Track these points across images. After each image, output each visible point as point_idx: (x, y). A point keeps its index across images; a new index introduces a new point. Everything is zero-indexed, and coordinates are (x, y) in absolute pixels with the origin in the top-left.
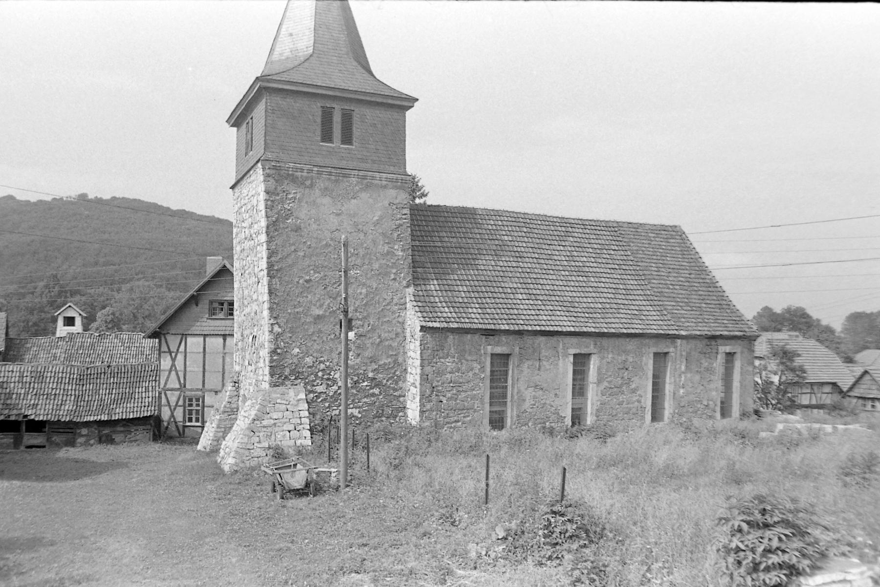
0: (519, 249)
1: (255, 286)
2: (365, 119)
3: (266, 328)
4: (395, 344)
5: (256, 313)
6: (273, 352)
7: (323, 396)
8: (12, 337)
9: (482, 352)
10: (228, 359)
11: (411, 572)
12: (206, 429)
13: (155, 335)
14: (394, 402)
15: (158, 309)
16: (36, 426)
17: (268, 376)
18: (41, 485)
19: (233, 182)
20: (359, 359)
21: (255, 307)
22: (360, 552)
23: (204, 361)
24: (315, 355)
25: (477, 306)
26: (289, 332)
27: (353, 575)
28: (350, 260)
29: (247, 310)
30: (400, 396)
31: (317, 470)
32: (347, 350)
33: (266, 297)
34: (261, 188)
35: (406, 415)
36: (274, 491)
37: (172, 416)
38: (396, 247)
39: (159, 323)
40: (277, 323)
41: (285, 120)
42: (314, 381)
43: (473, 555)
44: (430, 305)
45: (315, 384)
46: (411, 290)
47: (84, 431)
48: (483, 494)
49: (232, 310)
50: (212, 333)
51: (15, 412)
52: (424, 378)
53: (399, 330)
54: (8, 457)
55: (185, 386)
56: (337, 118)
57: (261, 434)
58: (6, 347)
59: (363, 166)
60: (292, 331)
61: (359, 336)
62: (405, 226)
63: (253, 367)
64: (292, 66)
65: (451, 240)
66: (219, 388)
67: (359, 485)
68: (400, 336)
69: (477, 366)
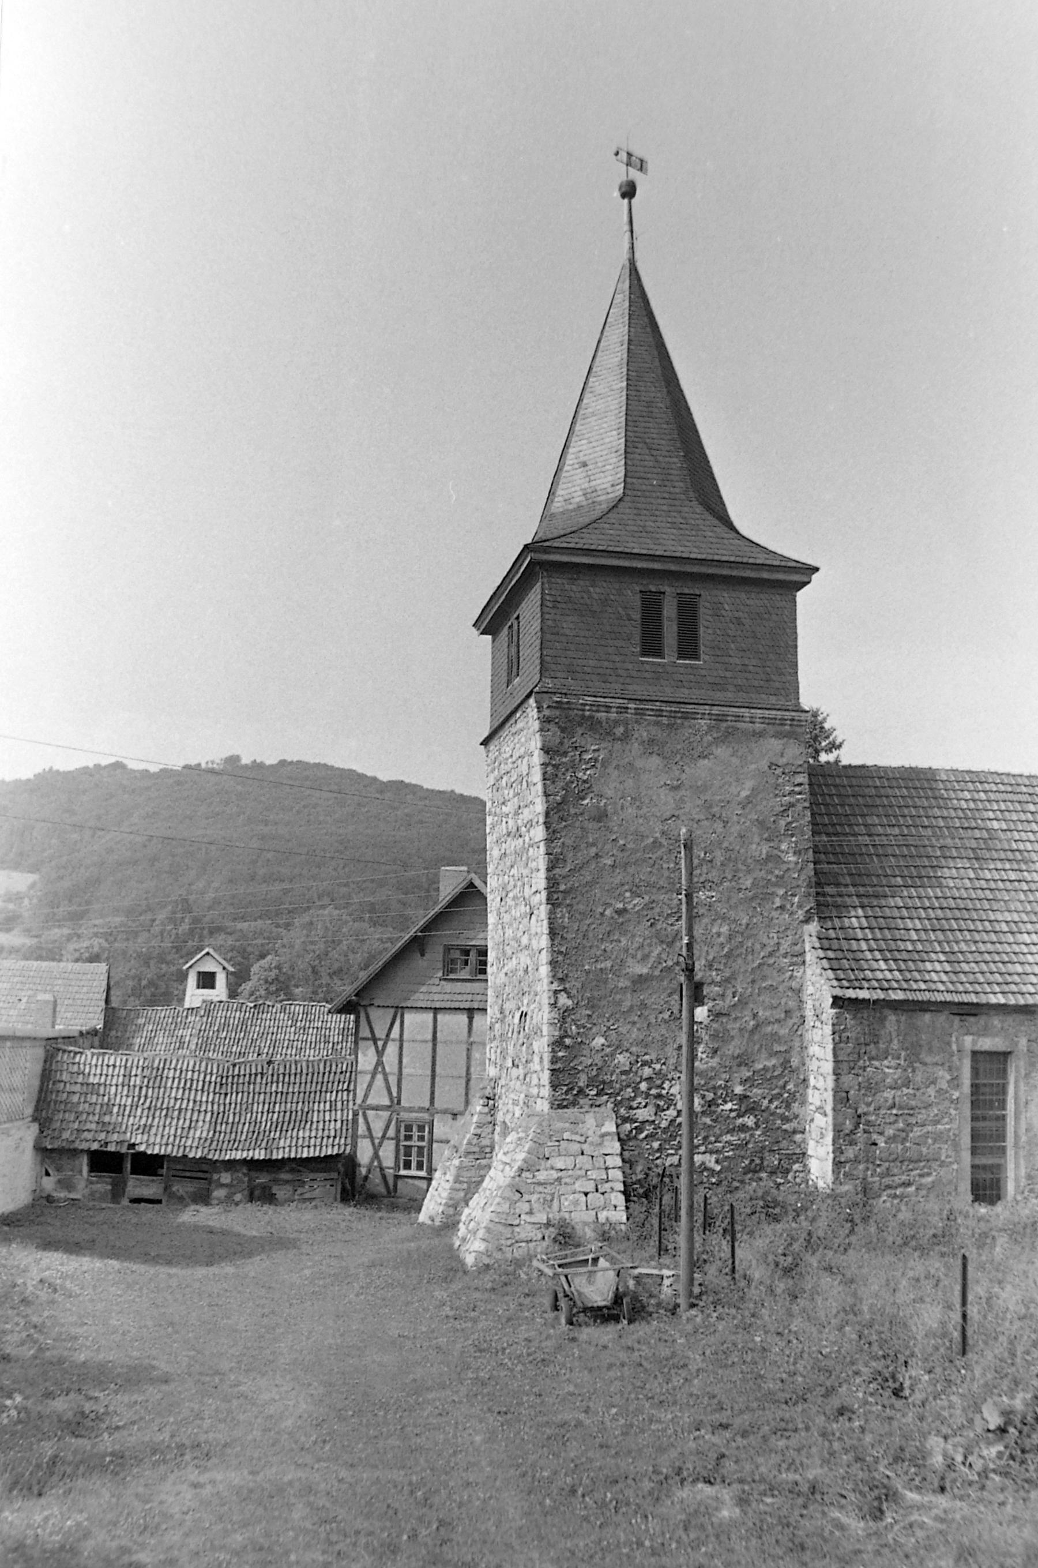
0: (1021, 846)
1: (526, 920)
2: (719, 609)
3: (545, 999)
4: (783, 1032)
5: (526, 971)
6: (557, 1043)
7: (649, 1129)
8: (113, 1005)
9: (954, 1047)
10: (476, 1055)
11: (813, 1489)
12: (434, 1183)
13: (348, 1008)
14: (784, 1144)
15: (357, 958)
16: (148, 1164)
17: (548, 1087)
18: (152, 1271)
19: (486, 734)
20: (717, 1060)
21: (524, 959)
22: (715, 1439)
23: (434, 1058)
24: (634, 1049)
25: (942, 958)
26: (586, 1007)
27: (700, 1485)
28: (697, 872)
29: (511, 965)
30: (794, 1132)
31: (636, 1272)
32: (693, 1040)
33: (544, 941)
34: (536, 743)
35: (806, 1170)
36: (556, 1308)
37: (376, 1156)
38: (784, 847)
39: (355, 985)
40: (565, 990)
41: (575, 619)
42: (634, 1099)
43: (937, 1460)
44: (850, 955)
45: (634, 1104)
46: (813, 927)
47: (226, 1178)
48: (956, 1335)
49: (485, 963)
50: (448, 1005)
51: (115, 1137)
52: (842, 1098)
53: (792, 1004)
54: (101, 1217)
55: (399, 1102)
56: (669, 610)
57: (534, 1198)
58: (105, 1026)
59: (719, 696)
60: (592, 1004)
61: (716, 1015)
62: (799, 807)
63: (521, 1071)
64: (587, 520)
65: (889, 831)
66: (459, 1107)
67: (715, 1303)
68: (793, 1015)
69: (944, 1076)
